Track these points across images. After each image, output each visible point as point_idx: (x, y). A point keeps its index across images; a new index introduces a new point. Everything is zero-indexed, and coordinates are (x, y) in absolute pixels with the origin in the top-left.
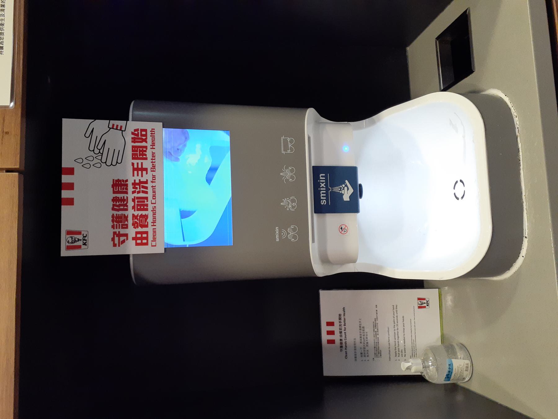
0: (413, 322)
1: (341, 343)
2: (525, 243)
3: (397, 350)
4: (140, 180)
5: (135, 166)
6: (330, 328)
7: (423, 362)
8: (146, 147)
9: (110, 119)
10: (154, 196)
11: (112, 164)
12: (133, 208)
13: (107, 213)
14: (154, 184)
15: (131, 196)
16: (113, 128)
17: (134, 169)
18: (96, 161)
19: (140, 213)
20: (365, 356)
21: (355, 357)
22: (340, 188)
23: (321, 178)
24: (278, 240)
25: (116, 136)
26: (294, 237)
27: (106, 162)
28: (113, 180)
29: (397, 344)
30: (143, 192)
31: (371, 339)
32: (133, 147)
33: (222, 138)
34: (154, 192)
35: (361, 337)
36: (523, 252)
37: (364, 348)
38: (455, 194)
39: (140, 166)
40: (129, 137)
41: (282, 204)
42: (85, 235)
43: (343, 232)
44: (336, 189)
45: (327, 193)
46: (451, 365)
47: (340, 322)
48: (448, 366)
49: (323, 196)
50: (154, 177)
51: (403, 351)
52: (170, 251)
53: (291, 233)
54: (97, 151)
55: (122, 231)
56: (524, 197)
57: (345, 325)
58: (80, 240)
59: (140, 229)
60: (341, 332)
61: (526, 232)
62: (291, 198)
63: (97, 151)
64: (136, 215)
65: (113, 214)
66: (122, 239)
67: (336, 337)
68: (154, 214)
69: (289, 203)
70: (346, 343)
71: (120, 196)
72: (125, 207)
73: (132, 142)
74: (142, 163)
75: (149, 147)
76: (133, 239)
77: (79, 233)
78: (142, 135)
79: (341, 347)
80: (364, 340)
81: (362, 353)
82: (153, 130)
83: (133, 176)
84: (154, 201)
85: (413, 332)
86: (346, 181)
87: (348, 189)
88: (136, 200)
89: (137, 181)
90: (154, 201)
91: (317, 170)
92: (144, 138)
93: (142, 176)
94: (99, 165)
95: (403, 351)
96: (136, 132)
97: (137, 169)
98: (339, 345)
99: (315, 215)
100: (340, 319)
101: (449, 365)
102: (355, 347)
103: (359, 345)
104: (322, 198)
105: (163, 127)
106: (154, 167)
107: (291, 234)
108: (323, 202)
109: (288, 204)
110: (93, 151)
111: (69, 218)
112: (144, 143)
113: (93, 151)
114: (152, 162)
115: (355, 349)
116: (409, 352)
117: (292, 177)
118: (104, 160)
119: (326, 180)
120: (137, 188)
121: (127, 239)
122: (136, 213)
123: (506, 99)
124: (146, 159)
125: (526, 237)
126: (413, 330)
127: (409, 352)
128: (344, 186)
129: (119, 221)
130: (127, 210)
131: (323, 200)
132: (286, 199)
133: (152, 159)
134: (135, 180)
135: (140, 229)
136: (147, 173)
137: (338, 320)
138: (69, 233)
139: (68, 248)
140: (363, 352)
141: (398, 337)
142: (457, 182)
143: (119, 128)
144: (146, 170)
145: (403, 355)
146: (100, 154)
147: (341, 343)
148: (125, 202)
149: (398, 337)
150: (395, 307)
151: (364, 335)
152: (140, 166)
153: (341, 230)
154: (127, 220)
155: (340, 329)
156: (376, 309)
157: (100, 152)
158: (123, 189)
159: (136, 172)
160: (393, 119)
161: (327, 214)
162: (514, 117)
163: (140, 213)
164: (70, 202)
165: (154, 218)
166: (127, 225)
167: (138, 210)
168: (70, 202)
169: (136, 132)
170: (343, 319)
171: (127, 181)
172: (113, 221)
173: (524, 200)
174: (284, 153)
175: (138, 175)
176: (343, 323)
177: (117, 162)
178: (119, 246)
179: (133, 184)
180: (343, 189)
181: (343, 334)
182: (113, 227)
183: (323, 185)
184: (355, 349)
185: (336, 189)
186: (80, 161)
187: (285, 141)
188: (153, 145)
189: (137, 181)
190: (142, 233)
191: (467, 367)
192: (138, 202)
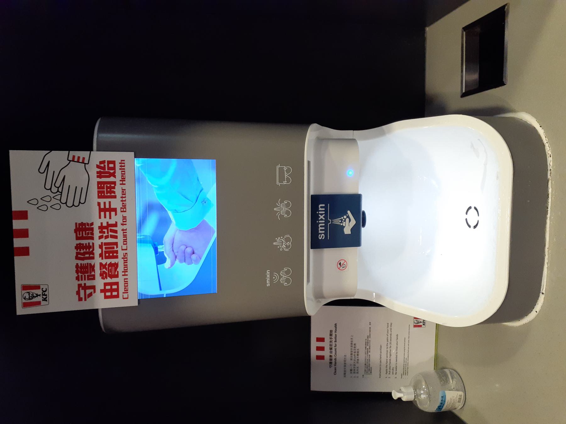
0: (407, 341)
1: (331, 360)
2: (542, 298)
3: (388, 368)
4: (107, 223)
5: (102, 206)
6: (320, 344)
7: (415, 390)
8: (114, 183)
9: (69, 149)
10: (125, 241)
11: (73, 205)
12: (101, 255)
13: (71, 263)
14: (124, 227)
15: (97, 242)
16: (73, 161)
17: (101, 210)
18: (54, 201)
19: (109, 261)
20: (354, 373)
21: (345, 374)
22: (342, 220)
23: (320, 209)
24: (268, 285)
25: (79, 169)
26: (287, 281)
27: (66, 203)
28: (76, 224)
29: (388, 362)
30: (112, 237)
31: (362, 357)
32: (99, 183)
33: (205, 175)
34: (125, 236)
35: (351, 354)
36: (538, 307)
37: (355, 365)
38: (466, 219)
39: (107, 206)
40: (93, 171)
41: (274, 243)
42: (44, 290)
43: (341, 268)
44: (337, 221)
45: (326, 226)
46: (444, 397)
47: (331, 338)
48: (440, 399)
49: (321, 230)
50: (124, 218)
51: (395, 369)
52: (146, 302)
53: (284, 277)
54: (54, 189)
55: (89, 283)
56: (546, 250)
57: (335, 342)
58: (39, 295)
59: (109, 280)
60: (331, 349)
61: (544, 289)
62: (285, 236)
63: (54, 189)
64: (104, 264)
65: (77, 264)
66: (88, 292)
67: (326, 353)
68: (126, 262)
69: (283, 242)
70: (335, 359)
71: (84, 242)
72: (91, 256)
73: (98, 177)
74: (110, 202)
75: (118, 183)
76: (102, 291)
77: (38, 287)
78: (109, 168)
79: (331, 363)
80: (355, 358)
81: (352, 370)
82: (122, 162)
83: (100, 218)
84: (124, 247)
85: (406, 351)
86: (349, 212)
87: (350, 220)
88: (104, 247)
89: (105, 224)
90: (124, 247)
91: (316, 200)
92: (112, 171)
93: (110, 218)
94: (57, 207)
95: (395, 369)
96: (102, 165)
97: (105, 210)
98: (329, 361)
99: (311, 251)
100: (331, 335)
101: (442, 397)
102: (345, 363)
103: (349, 361)
104: (320, 232)
105: (135, 157)
106: (124, 206)
107: (283, 277)
108: (321, 237)
109: (282, 243)
110: (50, 189)
111: (24, 271)
112: (112, 177)
113: (50, 189)
114: (122, 201)
115: (345, 366)
116: (400, 370)
117: (287, 213)
118: (64, 200)
119: (326, 211)
120: (104, 232)
121: (95, 292)
122: (104, 261)
123: (541, 131)
124: (115, 197)
125: (543, 294)
126: (407, 348)
127: (400, 370)
128: (345, 217)
129: (84, 271)
130: (93, 258)
131: (321, 234)
132: (279, 238)
133: (122, 197)
134: (102, 223)
135: (109, 280)
136: (116, 214)
137: (329, 337)
138: (25, 288)
139: (25, 305)
140: (353, 369)
141: (390, 355)
142: (470, 208)
143: (81, 161)
144: (115, 210)
145: (394, 373)
146: (58, 193)
147: (331, 360)
148: (91, 250)
149: (390, 355)
150: (389, 325)
151: (355, 352)
152: (107, 206)
153: (339, 266)
154: (94, 270)
155: (331, 345)
156: (370, 326)
157: (58, 191)
158: (88, 234)
159: (102, 214)
160: (407, 135)
161: (325, 249)
162: (548, 156)
163: (109, 261)
164: (25, 251)
165: (126, 266)
166: (94, 276)
167: (107, 258)
168: (25, 251)
169: (102, 165)
170: (334, 335)
171: (92, 224)
172: (77, 272)
173: (546, 253)
174: (279, 184)
175: (105, 217)
176: (334, 340)
177: (80, 202)
178: (85, 300)
179: (99, 228)
180: (345, 221)
181: (333, 350)
182: (77, 278)
183: (321, 217)
184: (345, 366)
185: (337, 221)
186: (35, 202)
187: (281, 170)
188: (123, 179)
189: (105, 224)
190: (111, 284)
191: (460, 399)
192: (106, 248)
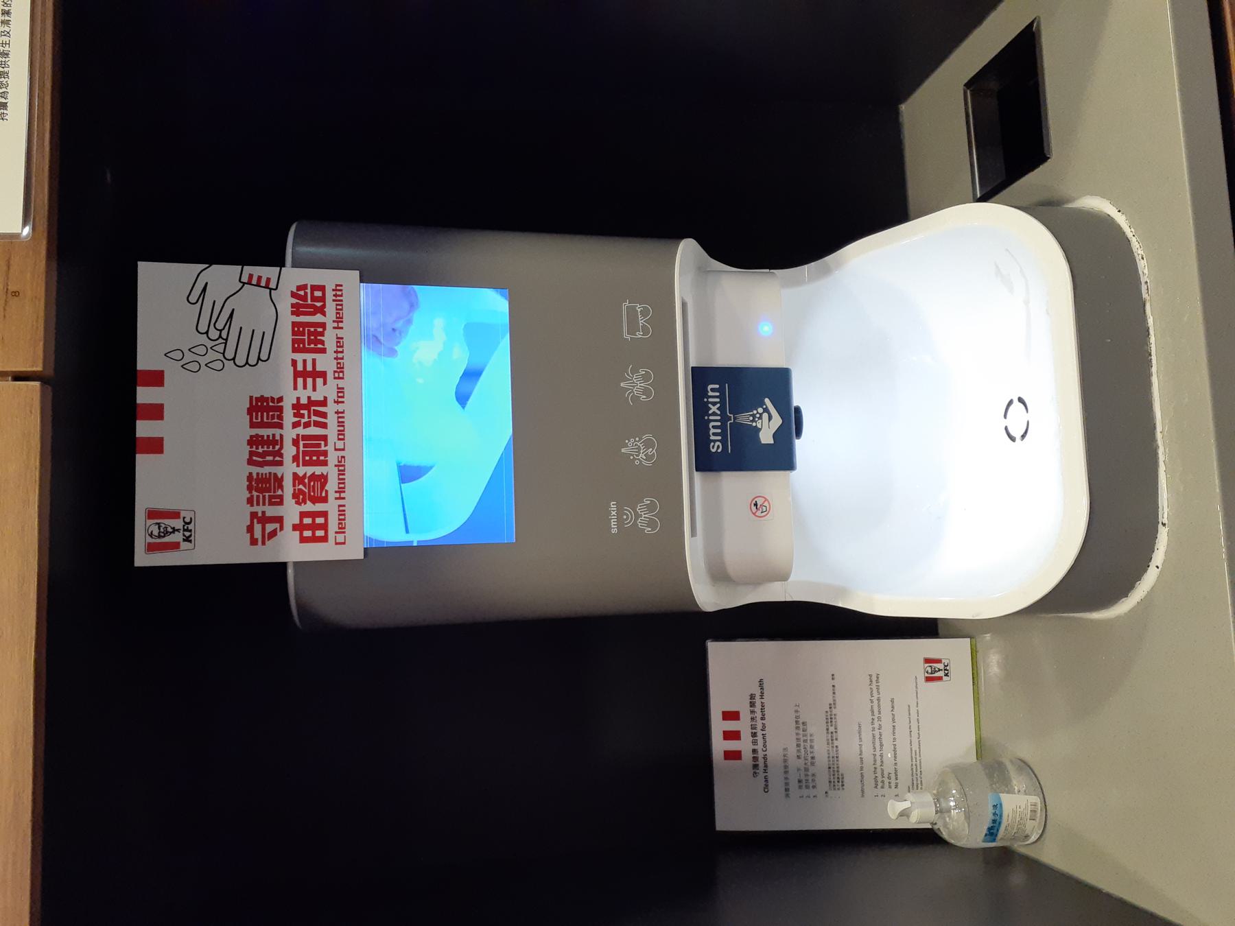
0: (913, 712)
1: (755, 759)
2: (1163, 538)
3: (879, 774)
4: (309, 398)
5: (300, 368)
6: (731, 726)
7: (937, 800)
8: (323, 325)
9: (243, 262)
10: (341, 434)
11: (247, 363)
12: (295, 459)
13: (237, 470)
14: (340, 407)
15: (289, 433)
16: (249, 283)
17: (297, 374)
18: (212, 355)
19: (310, 470)
20: (807, 787)
21: (787, 790)
22: (754, 416)
23: (710, 394)
24: (614, 531)
25: (256, 300)
26: (651, 523)
27: (234, 359)
28: (251, 398)
29: (878, 761)
30: (317, 424)
31: (820, 749)
32: (294, 324)
33: (492, 305)
34: (341, 424)
35: (798, 745)
36: (1159, 557)
37: (806, 770)
38: (1006, 428)
39: (309, 368)
40: (285, 303)
41: (623, 450)
42: (187, 520)
43: (759, 513)
44: (745, 418)
45: (723, 427)
46: (998, 807)
47: (752, 712)
48: (990, 810)
49: (714, 434)
50: (340, 390)
51: (893, 776)
52: (377, 554)
53: (645, 516)
54: (214, 334)
55: (271, 511)
56: (1159, 436)
57: (763, 719)
58: (178, 530)
59: (309, 507)
60: (754, 735)
61: (1164, 513)
62: (645, 437)
63: (214, 334)
64: (301, 474)
65: (251, 474)
66: (270, 527)
67: (744, 745)
68: (341, 473)
69: (639, 448)
70: (765, 758)
71: (265, 432)
72: (278, 459)
73: (293, 313)
74: (314, 361)
75: (330, 325)
76: (295, 528)
77: (175, 515)
78: (314, 299)
79: (755, 766)
80: (806, 752)
81: (802, 779)
82: (338, 288)
83: (295, 388)
84: (340, 445)
85: (915, 734)
86: (767, 401)
87: (770, 418)
88: (301, 443)
89: (304, 401)
90: (340, 445)
91: (701, 377)
92: (319, 304)
93: (314, 389)
94: (218, 365)
95: (893, 776)
96: (302, 293)
97: (304, 374)
98: (751, 763)
99: (697, 476)
100: (752, 704)
101: (995, 806)
102: (786, 767)
103: (794, 763)
104: (712, 438)
105: (361, 281)
106: (340, 369)
107: (643, 516)
108: (716, 447)
109: (638, 451)
110: (207, 333)
111: (153, 483)
112: (319, 315)
113: (207, 333)
114: (336, 358)
115: (786, 772)
116: (904, 779)
117: (646, 392)
118: (229, 355)
119: (722, 397)
120: (302, 416)
121: (282, 528)
122: (301, 471)
123: (1121, 220)
124: (323, 351)
125: (1164, 525)
126: (914, 729)
127: (904, 779)
128: (760, 410)
129: (264, 488)
130: (280, 463)
131: (715, 441)
132: (632, 440)
133: (336, 352)
134: (298, 399)
135: (309, 507)
136: (325, 383)
137: (748, 708)
138: (152, 514)
139: (151, 548)
140: (803, 778)
141: (881, 745)
142: (1011, 402)
143: (263, 284)
144: (323, 375)
145: (893, 785)
146: (221, 341)
147: (755, 759)
148: (277, 447)
149: (881, 745)
150: (874, 679)
151: (805, 741)
152: (309, 368)
153: (754, 508)
154: (281, 487)
155: (753, 727)
156: (833, 683)
157: (220, 336)
158: (273, 417)
159: (300, 381)
160: (871, 263)
161: (724, 474)
162: (1138, 258)
163: (310, 470)
164: (156, 446)
165: (342, 481)
166: (281, 497)
167: (306, 464)
168: (156, 446)
169: (302, 293)
170: (758, 705)
171: (280, 399)
172: (250, 488)
173: (1160, 442)
174: (629, 337)
175: (305, 387)
176: (759, 715)
177: (259, 359)
178: (263, 543)
179: (294, 407)
180: (760, 418)
181: (759, 738)
182: (250, 501)
183: (714, 409)
184: (786, 772)
185: (745, 418)
186: (178, 355)
187: (631, 311)
188: (339, 319)
189: (304, 401)
190: (313, 515)
191: (1034, 811)
192: (305, 446)
